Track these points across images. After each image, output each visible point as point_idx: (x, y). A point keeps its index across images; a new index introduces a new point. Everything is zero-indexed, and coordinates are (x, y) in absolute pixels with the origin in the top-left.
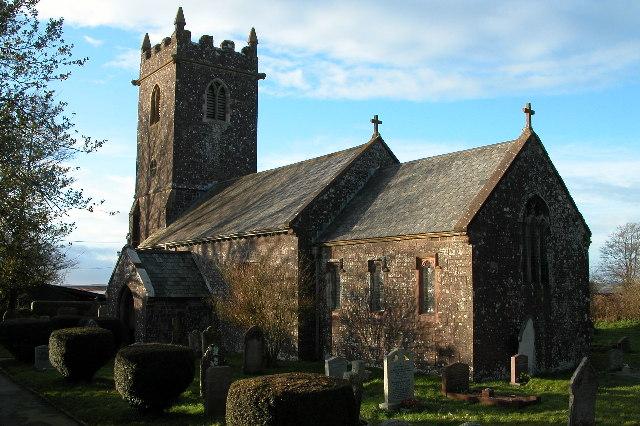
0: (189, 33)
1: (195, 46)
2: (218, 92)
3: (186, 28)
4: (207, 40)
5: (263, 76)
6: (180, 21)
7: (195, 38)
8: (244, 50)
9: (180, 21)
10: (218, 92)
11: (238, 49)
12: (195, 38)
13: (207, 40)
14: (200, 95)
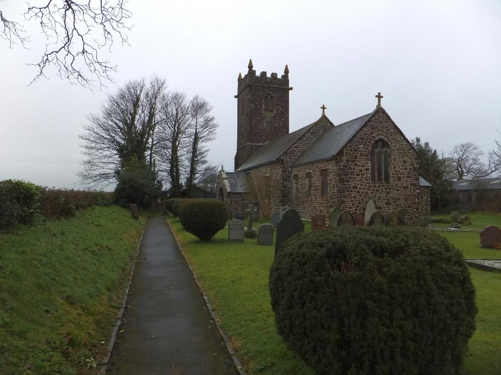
0: (255, 71)
1: (258, 78)
2: (269, 97)
3: (253, 69)
4: (264, 74)
5: (291, 89)
6: (250, 66)
7: (258, 74)
8: (283, 76)
9: (250, 66)
10: (269, 97)
11: (279, 76)
12: (258, 74)
13: (264, 74)
14: (261, 101)
